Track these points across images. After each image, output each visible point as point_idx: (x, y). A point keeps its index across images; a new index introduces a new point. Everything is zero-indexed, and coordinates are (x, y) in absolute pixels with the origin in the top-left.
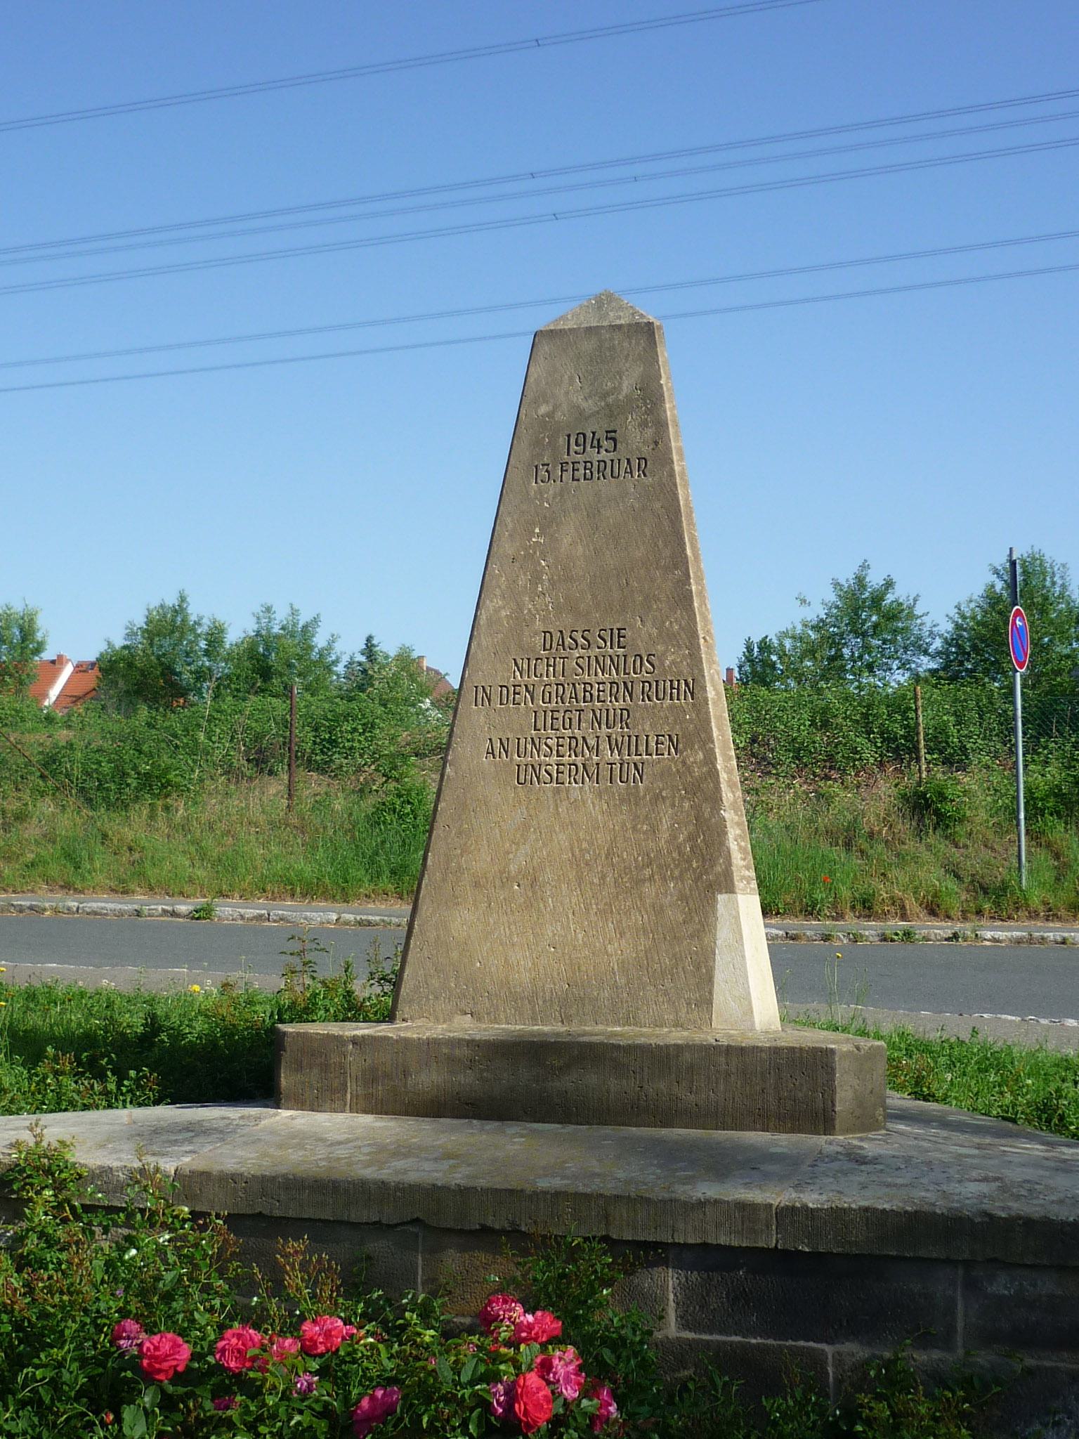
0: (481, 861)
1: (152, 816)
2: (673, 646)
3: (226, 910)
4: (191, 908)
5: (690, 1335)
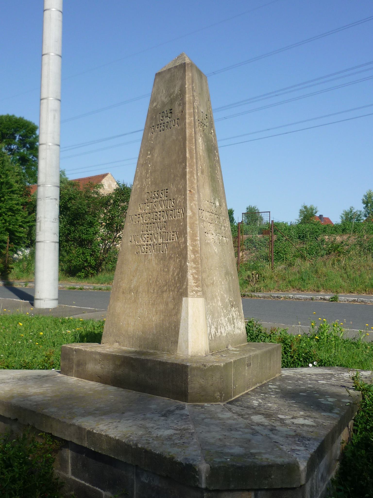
0: (124, 285)
1: (333, 264)
2: (180, 195)
3: (343, 298)
4: (330, 297)
5: (73, 478)
